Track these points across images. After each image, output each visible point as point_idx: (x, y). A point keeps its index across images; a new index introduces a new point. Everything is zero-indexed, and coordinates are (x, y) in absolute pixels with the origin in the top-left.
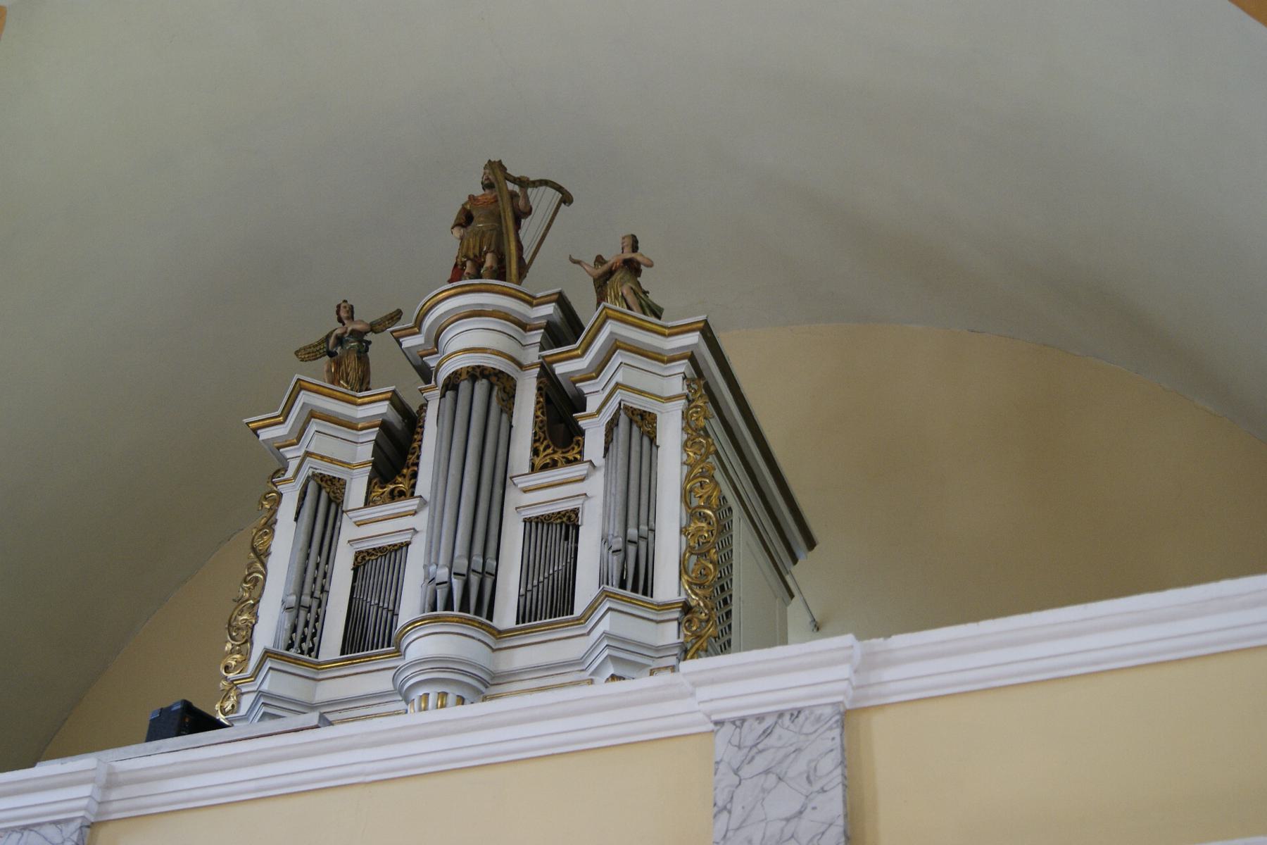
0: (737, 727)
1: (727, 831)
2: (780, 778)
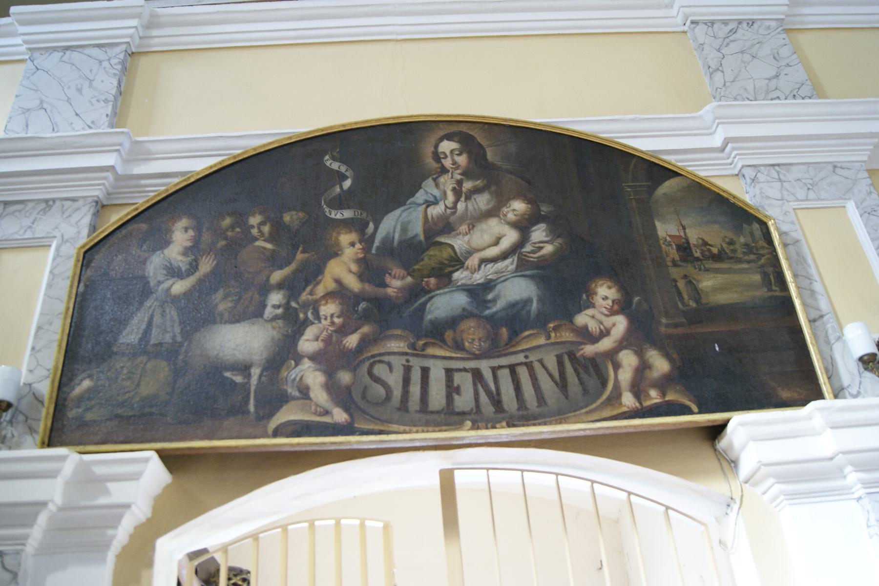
0: (709, 26)
1: (725, 82)
2: (753, 57)
